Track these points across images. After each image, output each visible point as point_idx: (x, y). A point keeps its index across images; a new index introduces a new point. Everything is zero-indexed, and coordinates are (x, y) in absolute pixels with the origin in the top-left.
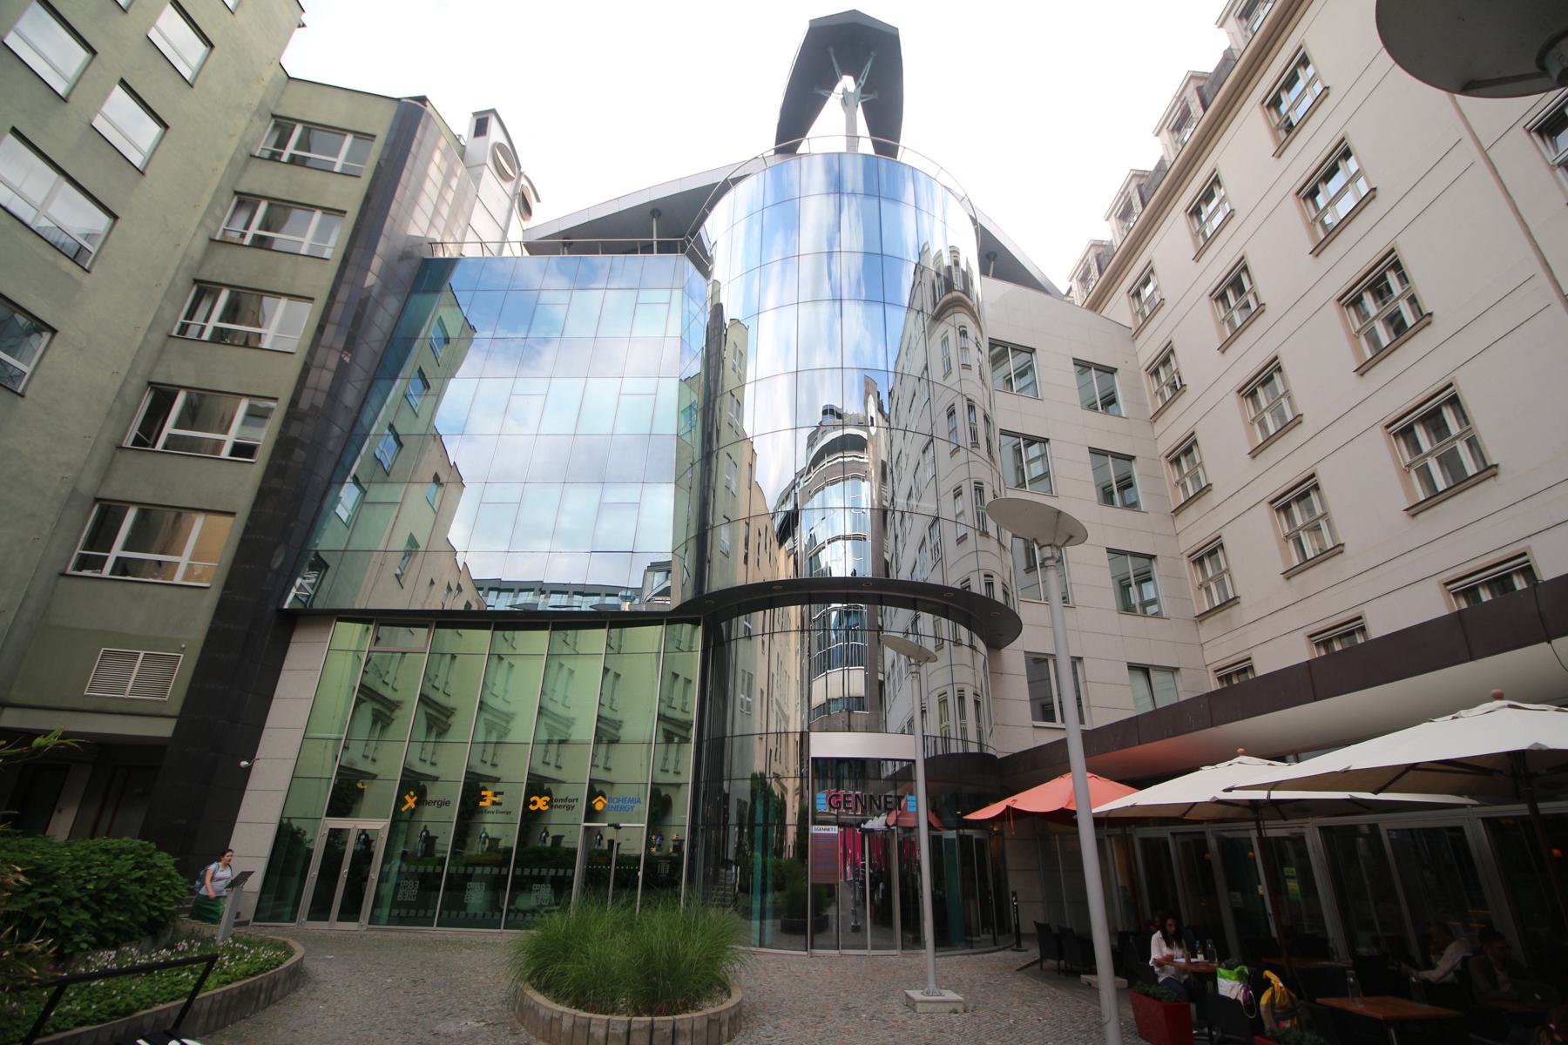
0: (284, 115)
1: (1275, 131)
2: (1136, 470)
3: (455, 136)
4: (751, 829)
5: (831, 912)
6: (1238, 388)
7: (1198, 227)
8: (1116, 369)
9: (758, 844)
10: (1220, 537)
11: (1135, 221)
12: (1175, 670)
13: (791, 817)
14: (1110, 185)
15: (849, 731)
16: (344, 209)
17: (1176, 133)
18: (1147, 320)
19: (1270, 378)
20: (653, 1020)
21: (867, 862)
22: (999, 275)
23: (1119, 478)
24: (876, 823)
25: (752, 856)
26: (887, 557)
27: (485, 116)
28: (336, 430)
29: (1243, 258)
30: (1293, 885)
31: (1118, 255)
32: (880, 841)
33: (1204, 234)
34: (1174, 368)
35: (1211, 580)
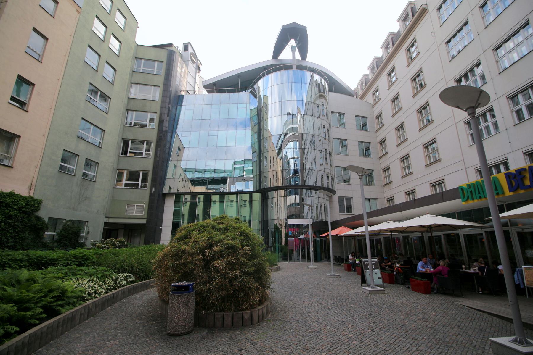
0: (138, 57)
1: (408, 59)
2: (371, 146)
4: (275, 239)
5: (293, 256)
6: (395, 128)
7: (390, 79)
9: (277, 242)
10: (435, 138)
11: (391, 50)
13: (283, 236)
14: (369, 61)
17: (404, 22)
18: (377, 102)
19: (426, 107)
20: (242, 313)
22: (336, 91)
24: (302, 237)
25: (276, 245)
28: (167, 147)
29: (398, 93)
31: (418, 13)
33: (391, 82)
34: (422, 78)
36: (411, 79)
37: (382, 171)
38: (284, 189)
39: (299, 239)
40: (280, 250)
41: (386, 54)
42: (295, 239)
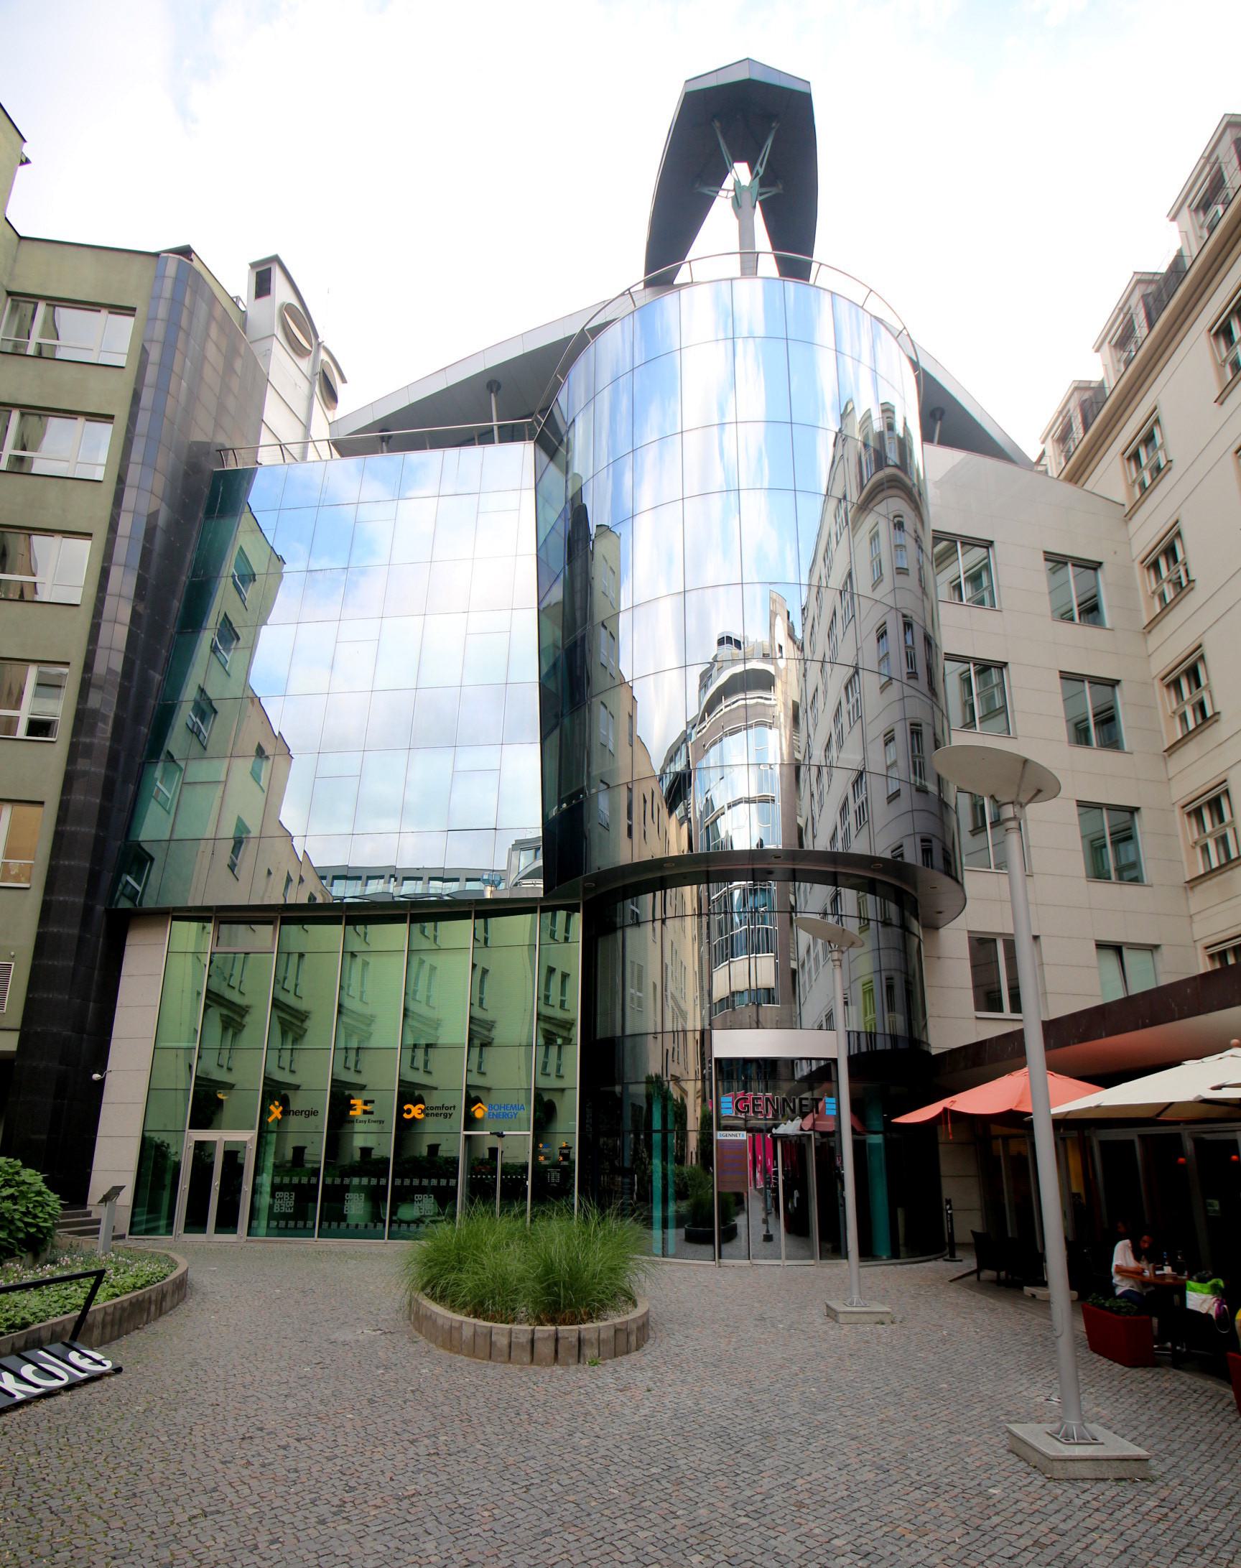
5: (740, 1221)
10: (1225, 781)
13: (693, 1122)
29: (1177, 522)
32: (795, 1147)
35: (1209, 836)
36: (1142, 562)
37: (1177, 811)
38: (698, 884)
39: (775, 1138)
40: (671, 1191)
41: (1060, 463)
42: (753, 1140)
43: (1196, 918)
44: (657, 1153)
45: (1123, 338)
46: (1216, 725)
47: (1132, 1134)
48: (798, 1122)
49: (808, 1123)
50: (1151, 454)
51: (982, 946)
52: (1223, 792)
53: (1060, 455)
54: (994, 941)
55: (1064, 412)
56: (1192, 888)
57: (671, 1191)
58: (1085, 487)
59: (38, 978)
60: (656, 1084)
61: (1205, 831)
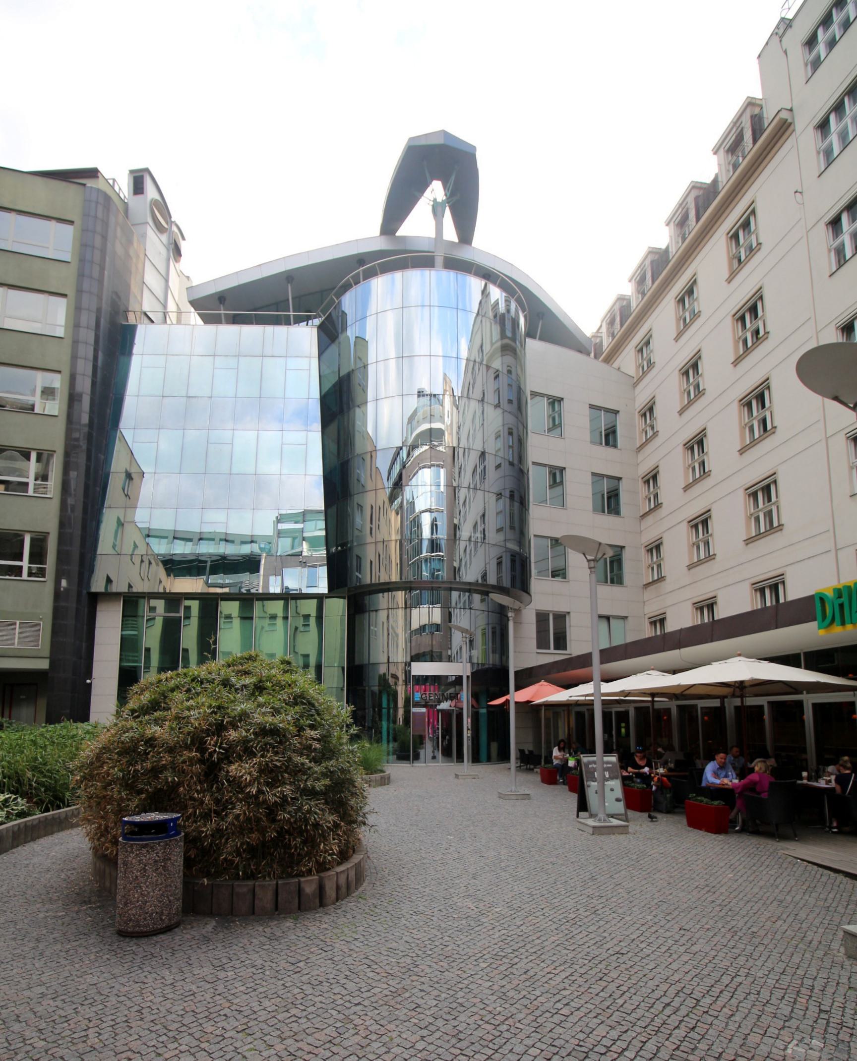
3: (106, 180)
5: (422, 752)
6: (684, 442)
8: (618, 411)
10: (775, 473)
12: (625, 618)
13: (401, 703)
15: (432, 661)
16: (66, 293)
21: (440, 727)
23: (609, 490)
26: (456, 564)
27: (140, 174)
30: (623, 730)
32: (446, 714)
35: (655, 563)
39: (438, 711)
40: (391, 738)
42: (428, 711)
43: (646, 603)
44: (385, 717)
45: (680, 221)
46: (660, 509)
47: (763, 701)
48: (449, 702)
49: (453, 704)
50: (747, 237)
51: (542, 618)
52: (772, 482)
53: (678, 236)
54: (549, 614)
55: (682, 204)
56: (646, 588)
57: (391, 738)
58: (613, 366)
59: (56, 630)
60: (383, 679)
61: (758, 507)
